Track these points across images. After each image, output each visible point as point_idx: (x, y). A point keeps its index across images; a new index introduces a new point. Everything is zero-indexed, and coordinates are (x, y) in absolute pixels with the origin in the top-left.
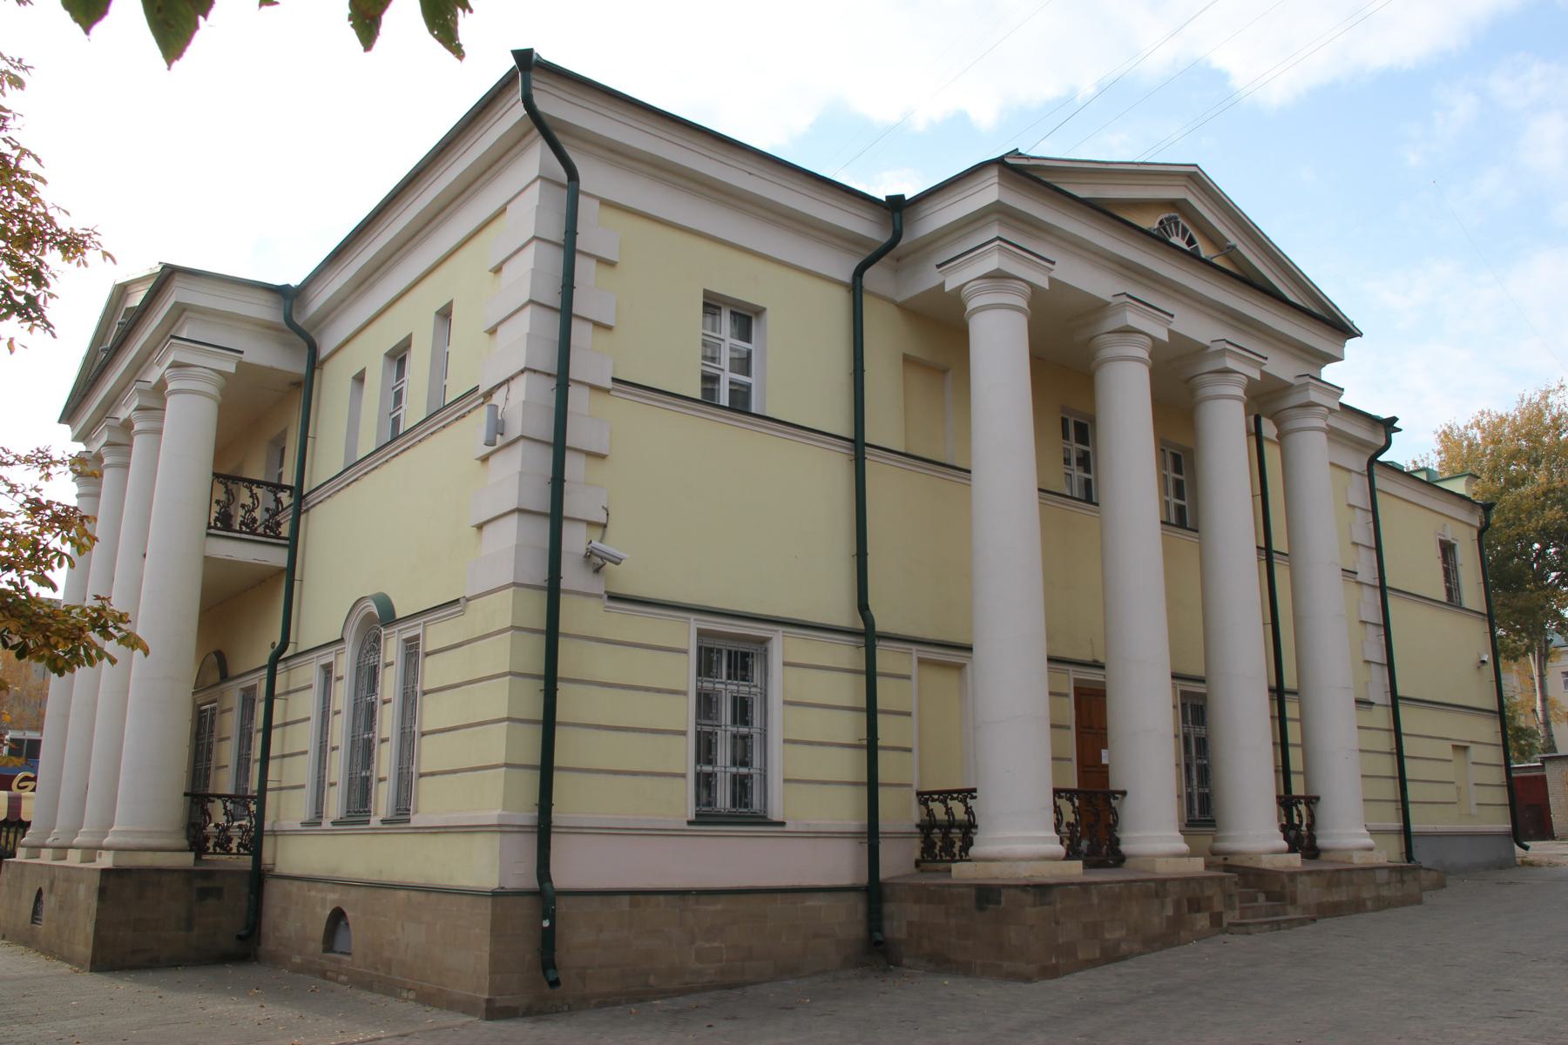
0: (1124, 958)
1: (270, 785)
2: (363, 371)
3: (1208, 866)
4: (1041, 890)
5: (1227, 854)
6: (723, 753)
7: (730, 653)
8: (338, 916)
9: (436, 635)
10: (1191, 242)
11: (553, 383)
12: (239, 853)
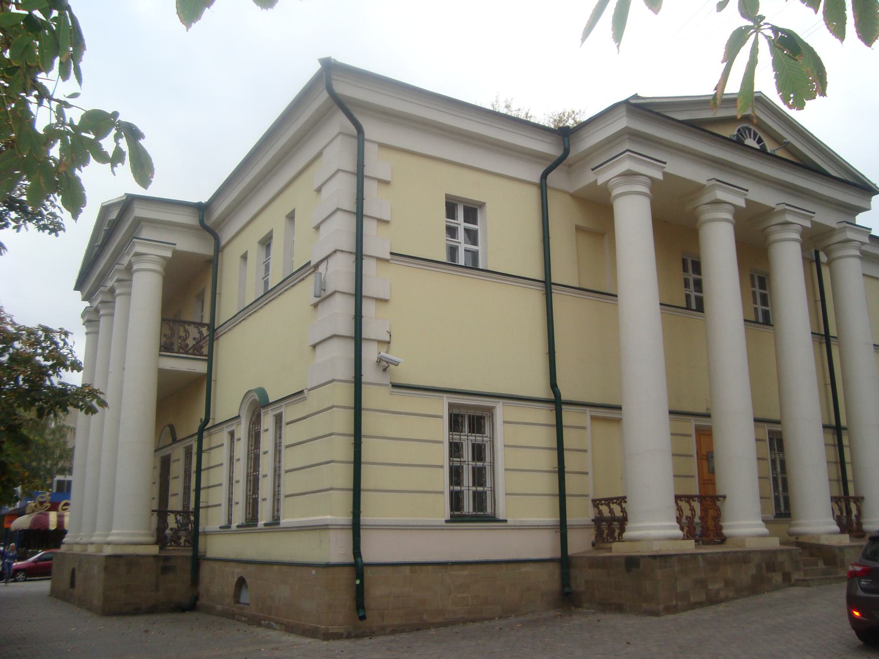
0: (722, 601)
1: (201, 505)
2: (246, 253)
3: (781, 544)
4: (663, 558)
5: (798, 535)
6: (467, 477)
7: (470, 416)
8: (241, 583)
9: (290, 413)
10: (760, 141)
11: (353, 258)
12: (185, 546)
